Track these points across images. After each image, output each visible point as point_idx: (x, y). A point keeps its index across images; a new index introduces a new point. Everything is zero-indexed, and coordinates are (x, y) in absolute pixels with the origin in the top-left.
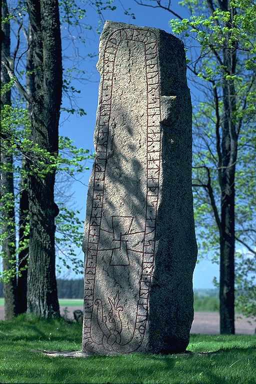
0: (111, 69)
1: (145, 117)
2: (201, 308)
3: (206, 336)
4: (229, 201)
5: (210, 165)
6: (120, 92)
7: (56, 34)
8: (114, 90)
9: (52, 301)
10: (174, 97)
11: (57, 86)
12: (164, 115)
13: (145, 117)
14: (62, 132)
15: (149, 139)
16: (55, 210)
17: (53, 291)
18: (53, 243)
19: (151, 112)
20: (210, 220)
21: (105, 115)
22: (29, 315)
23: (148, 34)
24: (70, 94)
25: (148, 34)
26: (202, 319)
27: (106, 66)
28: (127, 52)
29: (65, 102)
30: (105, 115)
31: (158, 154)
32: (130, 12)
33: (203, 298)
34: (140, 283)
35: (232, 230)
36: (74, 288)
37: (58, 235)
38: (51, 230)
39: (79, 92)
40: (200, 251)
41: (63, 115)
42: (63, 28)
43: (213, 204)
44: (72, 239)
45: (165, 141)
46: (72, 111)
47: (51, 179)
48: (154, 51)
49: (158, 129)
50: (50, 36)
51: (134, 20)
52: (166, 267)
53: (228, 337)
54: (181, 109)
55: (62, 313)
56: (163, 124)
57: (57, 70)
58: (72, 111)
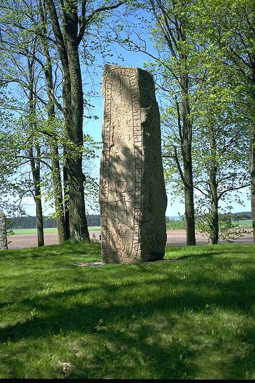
0: (109, 93)
1: (132, 121)
2: (176, 227)
3: (176, 247)
4: (188, 166)
5: (175, 144)
6: (116, 107)
7: (78, 71)
8: (112, 106)
9: (84, 232)
10: (61, 329)
11: (81, 102)
12: (143, 119)
13: (132, 121)
14: (85, 130)
15: (135, 134)
16: (84, 178)
17: (84, 222)
18: (83, 197)
19: (135, 118)
20: (176, 176)
21: (108, 121)
22: (72, 241)
23: (131, 71)
24: (88, 107)
25: (131, 71)
26: (178, 234)
27: (106, 92)
28: (119, 83)
29: (86, 112)
30: (108, 121)
31: (141, 143)
32: (121, 57)
33: (177, 221)
34: (134, 221)
35: (191, 182)
36: (96, 221)
37: (85, 191)
38: (82, 190)
39: (94, 107)
40: (169, 203)
41: (85, 120)
42: (83, 68)
43: (179, 167)
44: (94, 194)
45: (144, 136)
46: (90, 117)
47: (80, 161)
48: (135, 81)
49: (140, 127)
50: (74, 74)
51: (97, 120)
52: (149, 210)
53: (191, 247)
54: (153, 115)
55: (91, 237)
56: (142, 124)
57: (80, 93)
58: (90, 117)
